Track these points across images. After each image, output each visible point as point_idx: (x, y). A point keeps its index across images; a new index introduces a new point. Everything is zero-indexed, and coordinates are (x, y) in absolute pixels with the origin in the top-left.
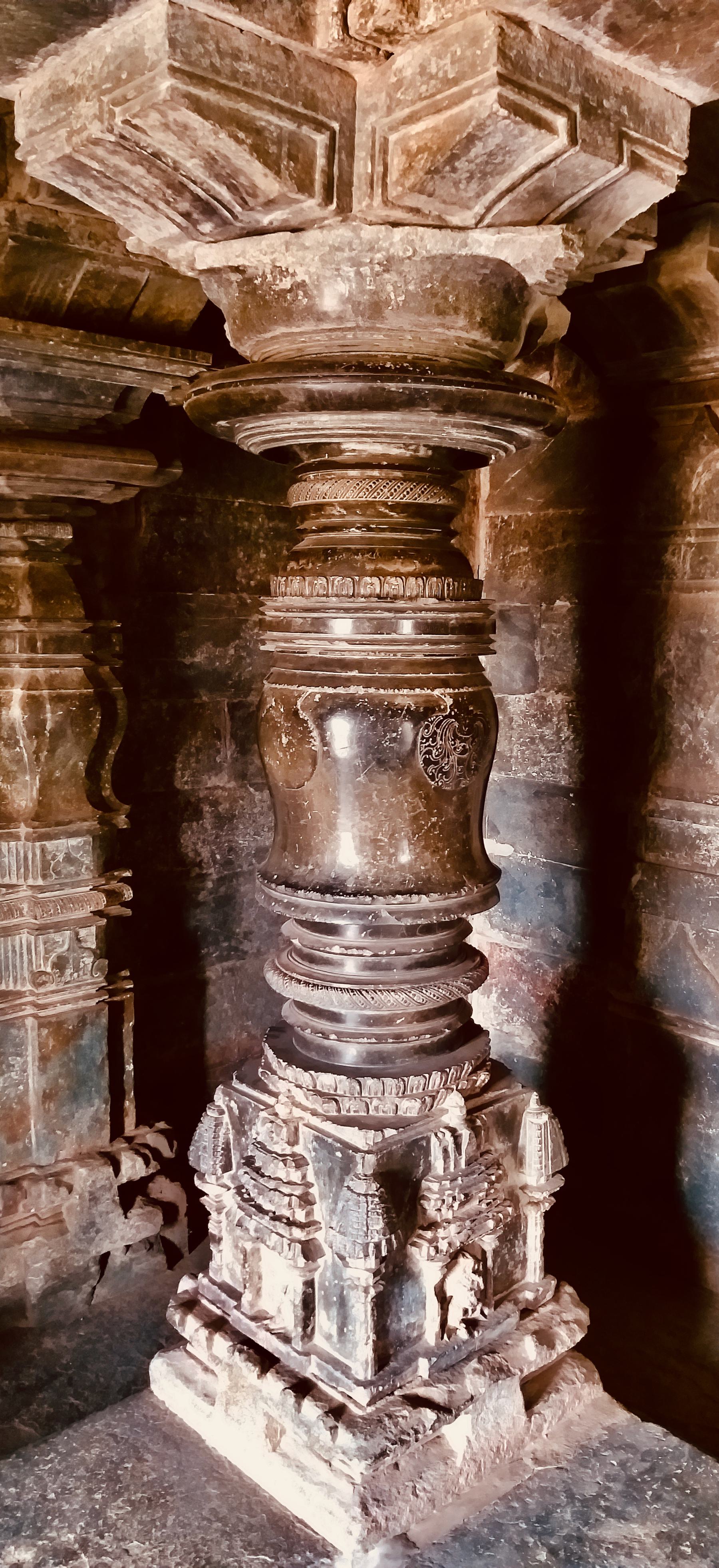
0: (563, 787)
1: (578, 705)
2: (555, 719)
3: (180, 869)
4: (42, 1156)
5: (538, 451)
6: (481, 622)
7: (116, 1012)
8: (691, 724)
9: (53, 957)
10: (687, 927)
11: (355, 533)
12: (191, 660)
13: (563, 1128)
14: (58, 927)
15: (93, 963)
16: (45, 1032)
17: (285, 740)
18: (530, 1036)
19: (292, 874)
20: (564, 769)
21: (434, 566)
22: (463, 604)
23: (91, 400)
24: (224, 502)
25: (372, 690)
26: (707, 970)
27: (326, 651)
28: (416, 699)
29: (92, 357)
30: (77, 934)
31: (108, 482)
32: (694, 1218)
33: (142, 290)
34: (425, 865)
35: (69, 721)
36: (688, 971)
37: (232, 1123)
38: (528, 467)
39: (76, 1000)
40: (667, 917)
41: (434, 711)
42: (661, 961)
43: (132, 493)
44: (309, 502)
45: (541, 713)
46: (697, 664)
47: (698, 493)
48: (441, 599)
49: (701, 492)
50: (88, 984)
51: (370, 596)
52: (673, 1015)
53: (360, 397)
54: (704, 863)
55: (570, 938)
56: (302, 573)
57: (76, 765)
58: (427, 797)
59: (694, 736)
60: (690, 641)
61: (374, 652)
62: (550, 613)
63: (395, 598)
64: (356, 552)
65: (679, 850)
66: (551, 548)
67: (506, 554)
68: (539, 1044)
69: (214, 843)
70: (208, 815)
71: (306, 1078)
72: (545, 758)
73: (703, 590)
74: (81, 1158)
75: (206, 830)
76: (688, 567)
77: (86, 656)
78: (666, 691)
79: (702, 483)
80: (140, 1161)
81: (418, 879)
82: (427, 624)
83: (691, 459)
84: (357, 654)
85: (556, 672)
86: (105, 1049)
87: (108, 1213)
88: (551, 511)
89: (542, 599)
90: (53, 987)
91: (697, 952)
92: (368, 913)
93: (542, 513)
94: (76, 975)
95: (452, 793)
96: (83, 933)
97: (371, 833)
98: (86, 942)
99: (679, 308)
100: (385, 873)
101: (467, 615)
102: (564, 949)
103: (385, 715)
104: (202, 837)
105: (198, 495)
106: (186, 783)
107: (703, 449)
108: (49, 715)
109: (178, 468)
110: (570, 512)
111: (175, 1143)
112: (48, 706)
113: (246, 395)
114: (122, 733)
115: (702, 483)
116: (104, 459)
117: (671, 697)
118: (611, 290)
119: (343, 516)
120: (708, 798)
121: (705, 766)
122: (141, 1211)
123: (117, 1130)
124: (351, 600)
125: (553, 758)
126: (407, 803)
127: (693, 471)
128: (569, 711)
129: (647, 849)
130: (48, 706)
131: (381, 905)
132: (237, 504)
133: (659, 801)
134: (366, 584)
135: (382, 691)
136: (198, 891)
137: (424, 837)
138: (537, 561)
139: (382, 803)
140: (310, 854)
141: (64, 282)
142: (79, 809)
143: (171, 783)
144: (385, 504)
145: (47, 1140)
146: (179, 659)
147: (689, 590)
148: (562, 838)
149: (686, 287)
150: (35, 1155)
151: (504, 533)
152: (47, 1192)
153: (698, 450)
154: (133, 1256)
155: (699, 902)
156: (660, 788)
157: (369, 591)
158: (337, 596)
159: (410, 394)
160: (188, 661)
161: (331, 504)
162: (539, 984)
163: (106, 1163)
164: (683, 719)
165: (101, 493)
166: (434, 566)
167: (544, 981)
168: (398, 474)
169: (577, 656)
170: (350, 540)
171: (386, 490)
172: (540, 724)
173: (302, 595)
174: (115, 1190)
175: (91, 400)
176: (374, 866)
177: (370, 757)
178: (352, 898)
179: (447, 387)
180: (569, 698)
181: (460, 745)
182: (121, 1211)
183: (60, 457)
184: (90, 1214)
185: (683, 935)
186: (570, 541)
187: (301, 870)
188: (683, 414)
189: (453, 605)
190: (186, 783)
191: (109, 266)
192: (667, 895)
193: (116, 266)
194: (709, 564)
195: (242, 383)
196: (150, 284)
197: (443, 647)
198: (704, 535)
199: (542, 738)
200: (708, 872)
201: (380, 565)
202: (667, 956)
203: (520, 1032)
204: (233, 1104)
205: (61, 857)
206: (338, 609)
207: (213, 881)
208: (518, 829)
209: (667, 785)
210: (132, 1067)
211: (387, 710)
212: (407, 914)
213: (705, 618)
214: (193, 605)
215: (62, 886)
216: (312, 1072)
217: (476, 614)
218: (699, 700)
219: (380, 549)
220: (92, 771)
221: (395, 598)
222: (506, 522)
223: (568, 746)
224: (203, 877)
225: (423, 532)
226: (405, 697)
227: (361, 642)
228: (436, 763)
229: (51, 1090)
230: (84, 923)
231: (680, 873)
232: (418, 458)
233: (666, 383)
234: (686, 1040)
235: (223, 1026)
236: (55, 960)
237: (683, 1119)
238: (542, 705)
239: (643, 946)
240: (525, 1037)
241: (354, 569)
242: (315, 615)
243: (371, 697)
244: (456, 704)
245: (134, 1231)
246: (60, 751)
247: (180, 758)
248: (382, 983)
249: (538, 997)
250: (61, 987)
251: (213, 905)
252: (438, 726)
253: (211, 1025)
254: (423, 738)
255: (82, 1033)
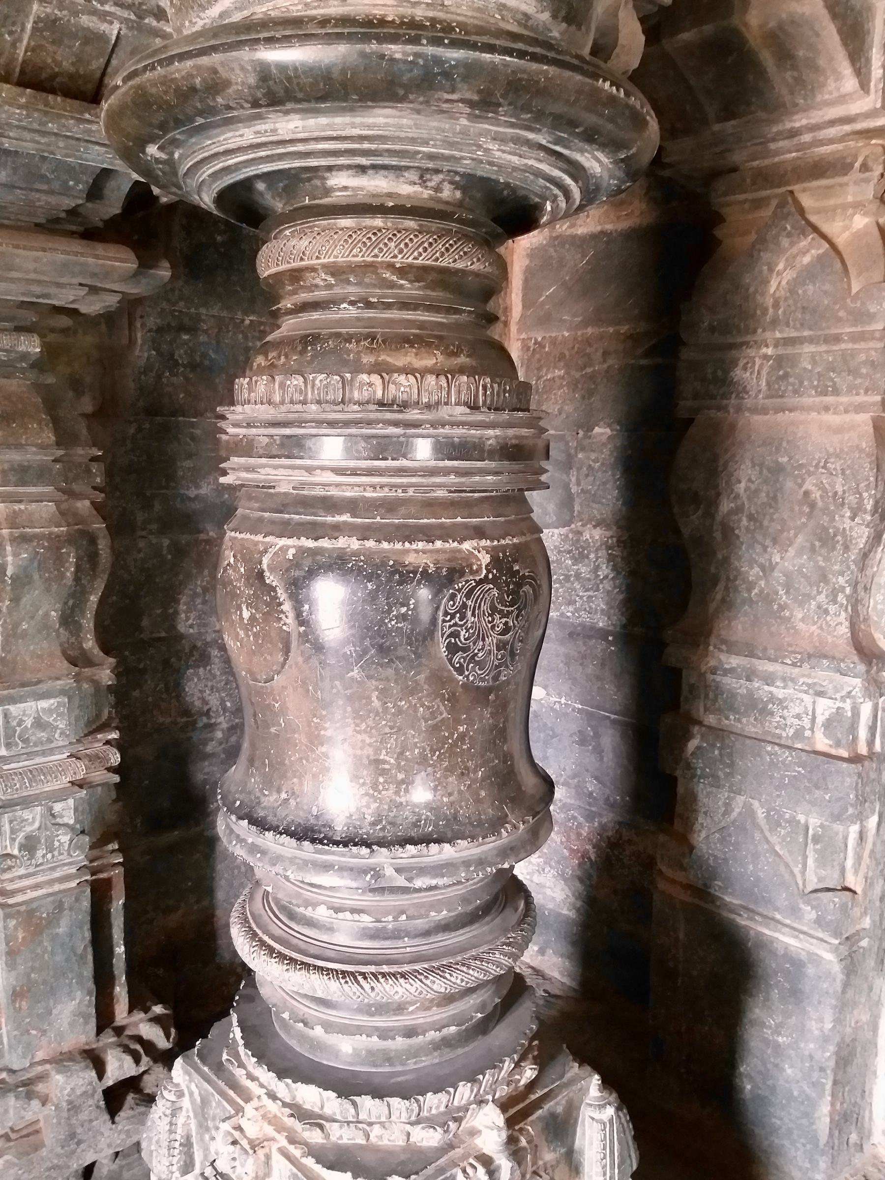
0: (601, 629)
1: (618, 541)
2: (592, 556)
3: (185, 719)
4: (14, 1059)
5: (576, 265)
6: (531, 442)
7: (100, 893)
8: (763, 568)
9: (21, 836)
10: (756, 804)
11: (348, 311)
12: (196, 492)
13: (638, 1137)
14: (26, 803)
15: (71, 841)
16: (12, 923)
17: (246, 614)
18: (563, 890)
19: (259, 803)
20: (602, 610)
21: (462, 359)
22: (505, 416)
23: (56, 185)
24: (232, 319)
25: (370, 544)
26: (779, 856)
27: (302, 485)
28: (435, 556)
29: (44, 124)
30: (51, 809)
31: (81, 284)
32: (757, 1131)
33: (113, 51)
34: (450, 795)
35: (36, 564)
36: (756, 856)
37: (194, 1111)
38: (564, 283)
39: (51, 882)
40: (731, 791)
41: (462, 573)
42: (723, 840)
43: (112, 301)
44: (282, 268)
45: (577, 549)
46: (775, 499)
47: (778, 294)
48: (474, 407)
49: (782, 293)
50: (65, 865)
51: (368, 402)
52: (735, 902)
53: (343, 72)
54: (777, 731)
55: (608, 791)
56: (271, 370)
57: (47, 615)
58: (453, 698)
59: (767, 582)
60: (765, 471)
61: (374, 487)
62: (587, 442)
63: (404, 406)
64: (348, 339)
65: (746, 714)
66: (589, 370)
67: (539, 378)
68: (572, 899)
69: (224, 689)
70: (217, 660)
71: (282, 1088)
72: (581, 597)
73: (783, 410)
74: (61, 1060)
75: (214, 677)
76: (763, 383)
77: (59, 489)
78: (733, 530)
79: (784, 283)
80: (128, 1060)
81: (438, 818)
82: (453, 445)
83: (769, 255)
84: (349, 489)
85: (594, 505)
86: (88, 935)
87: (91, 1121)
88: (590, 330)
89: (580, 426)
90: (22, 871)
91: (767, 834)
92: (364, 871)
93: (579, 333)
94: (49, 856)
95: (489, 690)
96: (58, 807)
97: (370, 751)
98: (62, 817)
99: (767, 58)
100: (390, 810)
101: (511, 432)
102: (601, 803)
103: (389, 580)
104: (210, 684)
105: (203, 311)
106: (191, 626)
107: (785, 242)
108: (10, 559)
109: (165, 269)
110: (611, 330)
111: (173, 1031)
112: (9, 548)
113: (165, 81)
114: (106, 577)
115: (784, 283)
116: (67, 253)
117: (738, 537)
118: (685, 36)
119: (329, 287)
120: (785, 657)
121: (780, 617)
122: (131, 1113)
123: (104, 1019)
124: (339, 408)
125: (590, 597)
126: (426, 706)
127: (771, 270)
128: (609, 548)
129: (706, 709)
130: (9, 548)
131: (382, 857)
132: (247, 322)
133: (723, 657)
134: (362, 385)
135: (385, 545)
136: (205, 743)
137: (445, 752)
138: (574, 385)
139: (386, 710)
140: (283, 776)
141: (11, 33)
142: (52, 666)
143: (174, 627)
144: (391, 266)
145: (19, 1042)
146: (182, 491)
147: (764, 411)
148: (599, 684)
149: (781, 26)
150: (7, 1057)
151: (537, 356)
152: (15, 1108)
153: (778, 244)
154: (124, 1163)
155: (772, 777)
156: (724, 642)
157: (366, 395)
158: (319, 402)
159: (424, 66)
160: (192, 493)
161: (313, 269)
162: (573, 837)
163: (87, 1067)
164: (752, 563)
165: (71, 298)
166: (462, 359)
167: (579, 835)
168: (411, 224)
169: (618, 488)
170: (341, 323)
171: (392, 245)
172: (576, 561)
173: (270, 403)
174: (99, 1095)
175: (56, 185)
176: (375, 799)
177: (367, 642)
178: (341, 849)
179: (487, 56)
180: (609, 533)
181: (499, 622)
182: (107, 1117)
183: (11, 249)
184: (70, 1125)
185: (750, 812)
186: (611, 361)
187: (272, 799)
188: (758, 204)
189: (492, 416)
190: (191, 626)
191: (65, 12)
192: (732, 765)
193: (76, 14)
194: (791, 380)
195: (160, 62)
196: (123, 42)
197: (477, 478)
198: (785, 345)
199: (578, 575)
200: (783, 742)
201: (383, 357)
202: (730, 835)
203: (552, 885)
204: (193, 1087)
205: (29, 722)
206: (320, 423)
207: (223, 730)
208: (551, 670)
209: (733, 638)
210: (123, 948)
211: (393, 574)
212: (423, 871)
213: (784, 444)
214: (198, 432)
215: (30, 755)
216: (289, 1081)
217: (525, 432)
218: (775, 541)
219: (383, 334)
220: (69, 620)
221: (404, 406)
222: (541, 345)
223: (607, 585)
224: (211, 727)
225: (449, 311)
226: (418, 554)
227: (354, 472)
228: (465, 649)
229: (22, 986)
230: (59, 795)
231: (748, 741)
232: (439, 200)
233: (735, 169)
234: (752, 933)
235: (236, 883)
236: (23, 841)
237: (745, 1020)
238: (578, 540)
239: (700, 820)
240: (558, 890)
241: (345, 363)
242: (287, 431)
243: (369, 555)
244: (496, 562)
245: (123, 1136)
246: (26, 600)
247: (184, 599)
248: (389, 962)
249: (572, 851)
250: (31, 870)
251: (223, 756)
252: (468, 595)
253: (223, 882)
254: (446, 613)
255: (58, 920)
